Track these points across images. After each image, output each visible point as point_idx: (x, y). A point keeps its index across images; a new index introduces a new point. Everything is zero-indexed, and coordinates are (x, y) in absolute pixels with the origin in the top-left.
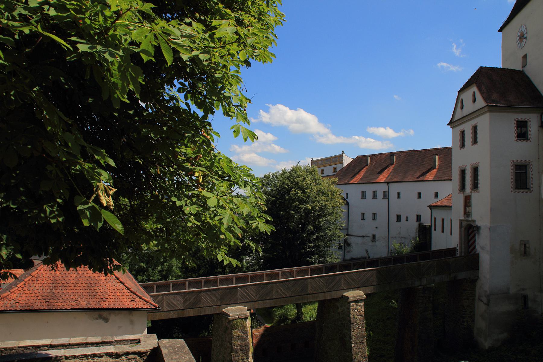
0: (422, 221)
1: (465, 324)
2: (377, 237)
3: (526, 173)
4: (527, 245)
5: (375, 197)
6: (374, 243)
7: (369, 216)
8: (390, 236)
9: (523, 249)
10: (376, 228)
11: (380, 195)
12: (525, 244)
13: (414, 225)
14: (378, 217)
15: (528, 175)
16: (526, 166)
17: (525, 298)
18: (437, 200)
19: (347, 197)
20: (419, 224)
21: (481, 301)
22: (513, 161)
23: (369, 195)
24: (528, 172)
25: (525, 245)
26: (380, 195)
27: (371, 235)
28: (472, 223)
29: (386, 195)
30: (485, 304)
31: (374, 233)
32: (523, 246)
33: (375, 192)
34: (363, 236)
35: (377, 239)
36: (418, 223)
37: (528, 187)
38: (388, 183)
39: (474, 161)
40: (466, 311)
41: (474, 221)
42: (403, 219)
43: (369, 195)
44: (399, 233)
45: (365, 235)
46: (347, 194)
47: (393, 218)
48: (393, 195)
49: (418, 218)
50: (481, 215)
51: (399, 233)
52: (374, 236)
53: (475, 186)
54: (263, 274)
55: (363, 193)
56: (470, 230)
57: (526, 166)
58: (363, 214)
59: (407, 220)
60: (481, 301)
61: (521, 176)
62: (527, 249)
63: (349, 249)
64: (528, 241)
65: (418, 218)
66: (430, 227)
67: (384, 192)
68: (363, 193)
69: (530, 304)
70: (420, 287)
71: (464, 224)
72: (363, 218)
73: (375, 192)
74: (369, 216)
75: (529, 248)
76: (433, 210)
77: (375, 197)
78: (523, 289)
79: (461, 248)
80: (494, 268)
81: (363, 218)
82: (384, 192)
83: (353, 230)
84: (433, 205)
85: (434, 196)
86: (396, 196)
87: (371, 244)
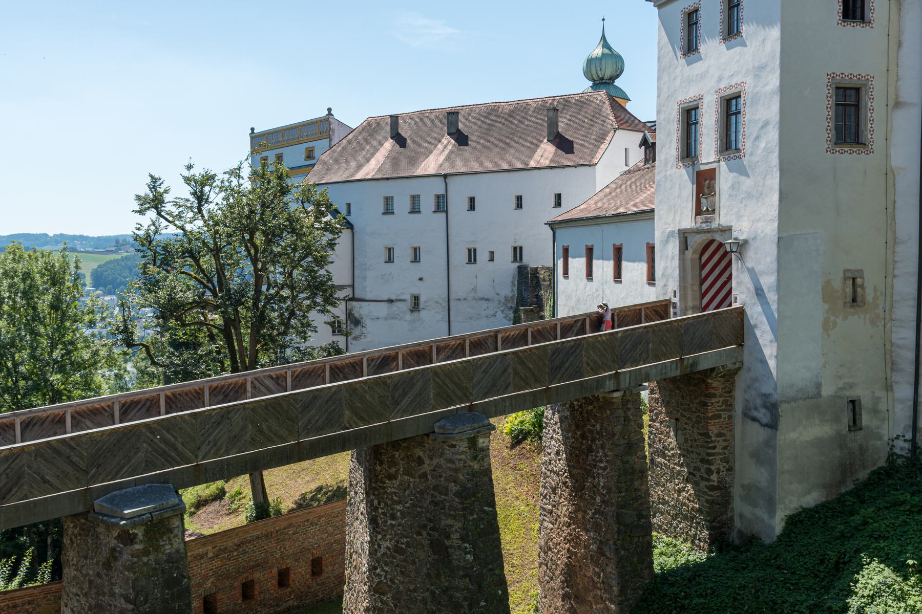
0: (526, 260)
1: (714, 477)
2: (422, 299)
3: (857, 106)
4: (859, 281)
5: (415, 209)
6: (416, 314)
7: (403, 255)
8: (453, 296)
9: (849, 290)
10: (421, 279)
11: (427, 204)
12: (854, 280)
13: (506, 266)
14: (423, 256)
15: (862, 111)
16: (857, 90)
17: (854, 404)
18: (559, 211)
19: (349, 213)
20: (519, 267)
21: (754, 419)
22: (831, 76)
23: (402, 205)
24: (862, 104)
25: (854, 279)
26: (427, 204)
27: (408, 297)
28: (719, 238)
29: (441, 203)
30: (766, 425)
31: (415, 291)
32: (851, 282)
33: (415, 199)
34: (391, 301)
35: (421, 306)
36: (517, 264)
37: (862, 140)
38: (445, 176)
39: (727, 85)
40: (714, 448)
41: (727, 230)
42: (482, 256)
43: (402, 205)
44: (474, 290)
45: (393, 297)
46: (349, 205)
47: (459, 256)
48: (457, 204)
49: (518, 253)
50: (751, 211)
51: (474, 290)
52: (416, 298)
53: (728, 144)
54: (202, 390)
55: (388, 200)
56: (711, 257)
57: (857, 90)
58: (390, 251)
59: (492, 260)
60: (754, 419)
61: (849, 114)
62: (859, 289)
63: (357, 331)
64: (861, 271)
65: (518, 253)
66: (552, 271)
67: (438, 197)
68: (388, 200)
69: (865, 419)
70: (616, 395)
71: (696, 242)
72: (390, 260)
73: (415, 199)
74: (403, 255)
75: (862, 286)
76: (558, 232)
77: (415, 209)
78: (851, 386)
79: (683, 297)
80: (784, 343)
81: (390, 260)
82: (438, 197)
83: (370, 287)
84: (560, 219)
85: (552, 202)
86: (466, 205)
87: (408, 316)
